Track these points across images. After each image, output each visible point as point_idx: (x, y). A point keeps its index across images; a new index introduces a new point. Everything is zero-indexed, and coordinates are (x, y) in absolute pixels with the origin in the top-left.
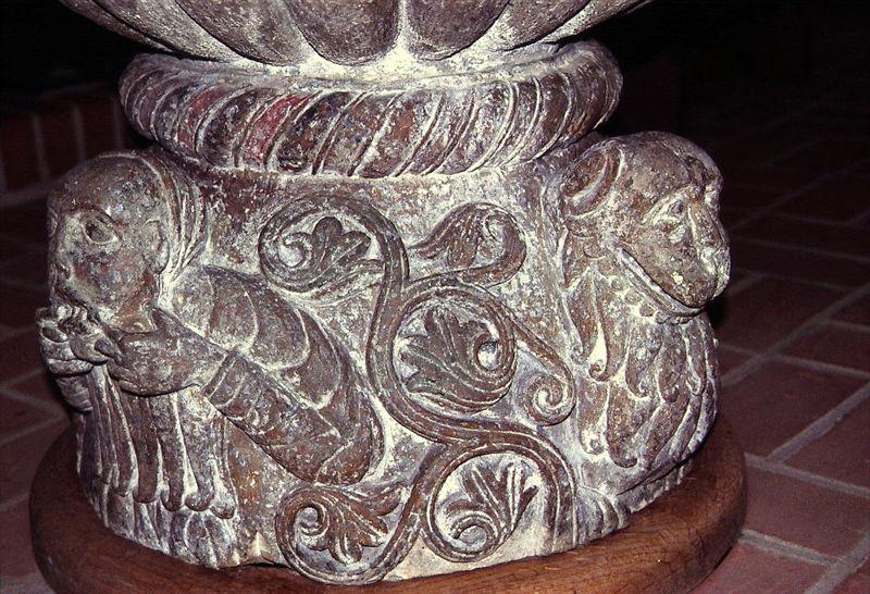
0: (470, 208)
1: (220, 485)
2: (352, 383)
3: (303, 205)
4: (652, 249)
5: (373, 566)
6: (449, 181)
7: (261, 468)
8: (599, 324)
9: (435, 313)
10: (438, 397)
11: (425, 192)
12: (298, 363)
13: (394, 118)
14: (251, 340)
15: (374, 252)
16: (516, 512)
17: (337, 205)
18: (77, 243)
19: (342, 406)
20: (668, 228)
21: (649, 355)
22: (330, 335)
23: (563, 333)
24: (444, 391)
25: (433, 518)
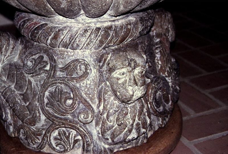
0: (77, 60)
1: (9, 117)
3: (37, 51)
5: (37, 147)
6: (74, 52)
8: (103, 100)
9: (58, 88)
10: (53, 110)
11: (67, 54)
12: (23, 93)
13: (54, 34)
14: (15, 84)
15: (48, 68)
16: (72, 144)
17: (44, 53)
21: (114, 112)
22: (34, 87)
24: (54, 109)
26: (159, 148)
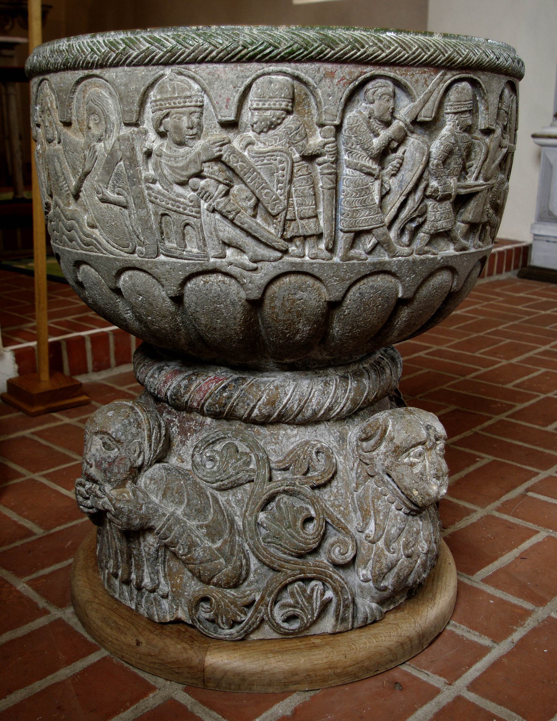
2: (234, 535)
4: (403, 475)
7: (184, 573)
8: (372, 512)
14: (183, 507)
18: (97, 450)
19: (227, 547)
20: (412, 465)
22: (225, 507)
23: (353, 514)
25: (271, 610)
26: (212, 629)
